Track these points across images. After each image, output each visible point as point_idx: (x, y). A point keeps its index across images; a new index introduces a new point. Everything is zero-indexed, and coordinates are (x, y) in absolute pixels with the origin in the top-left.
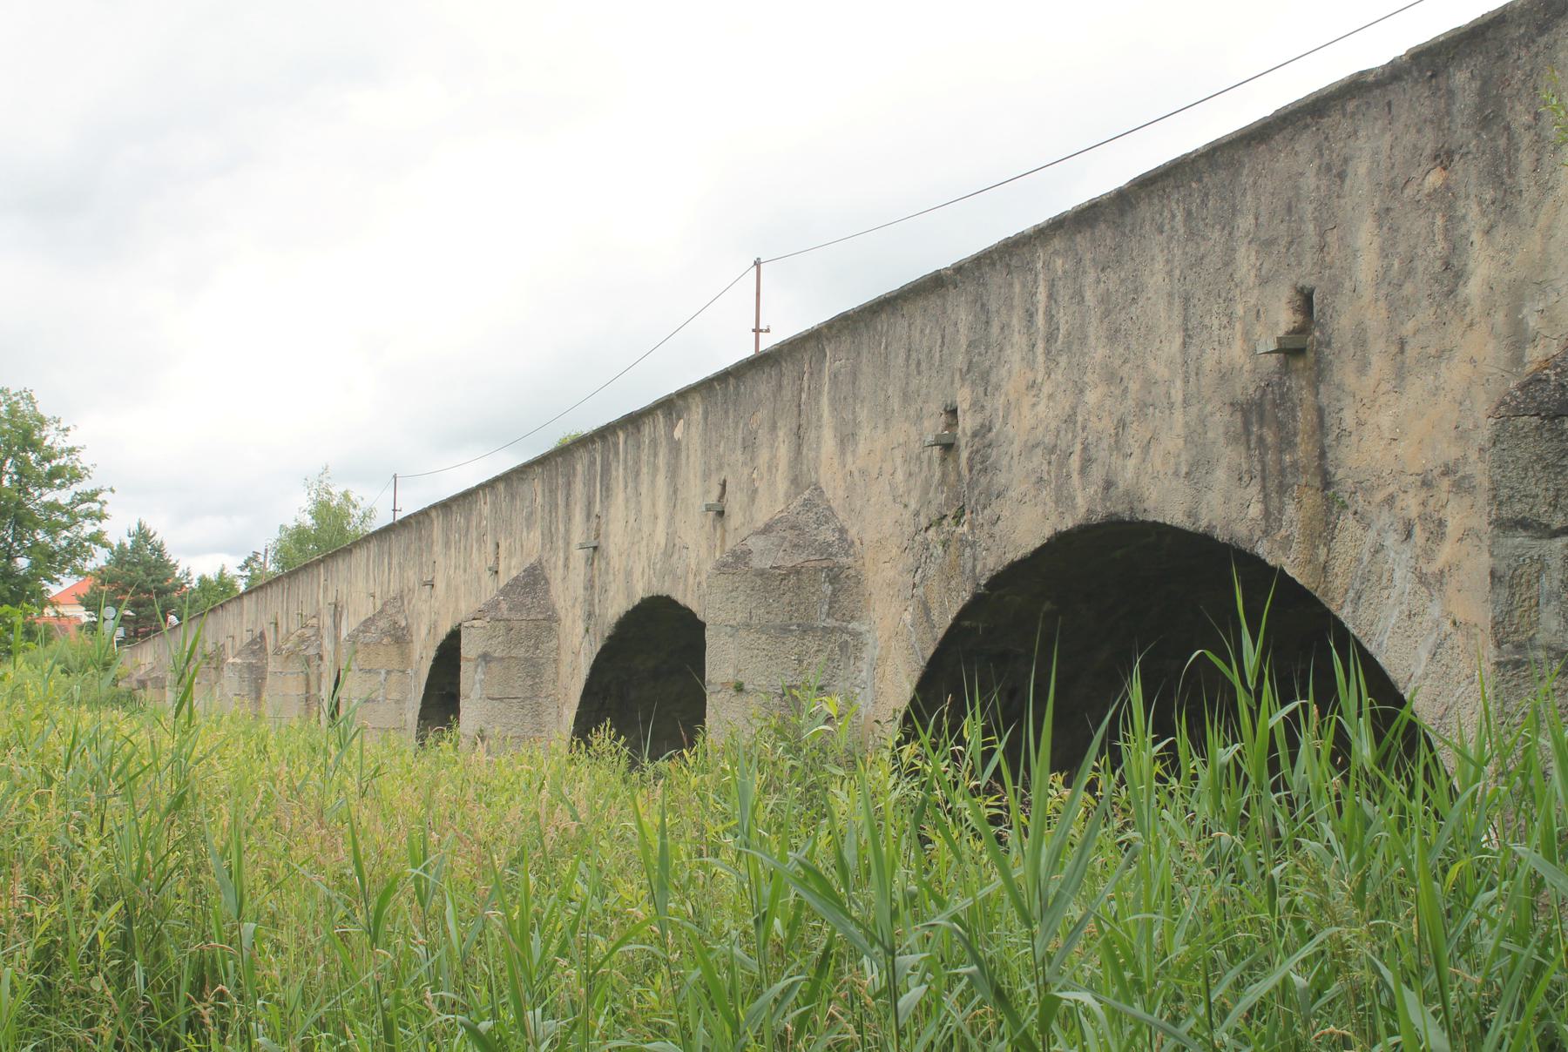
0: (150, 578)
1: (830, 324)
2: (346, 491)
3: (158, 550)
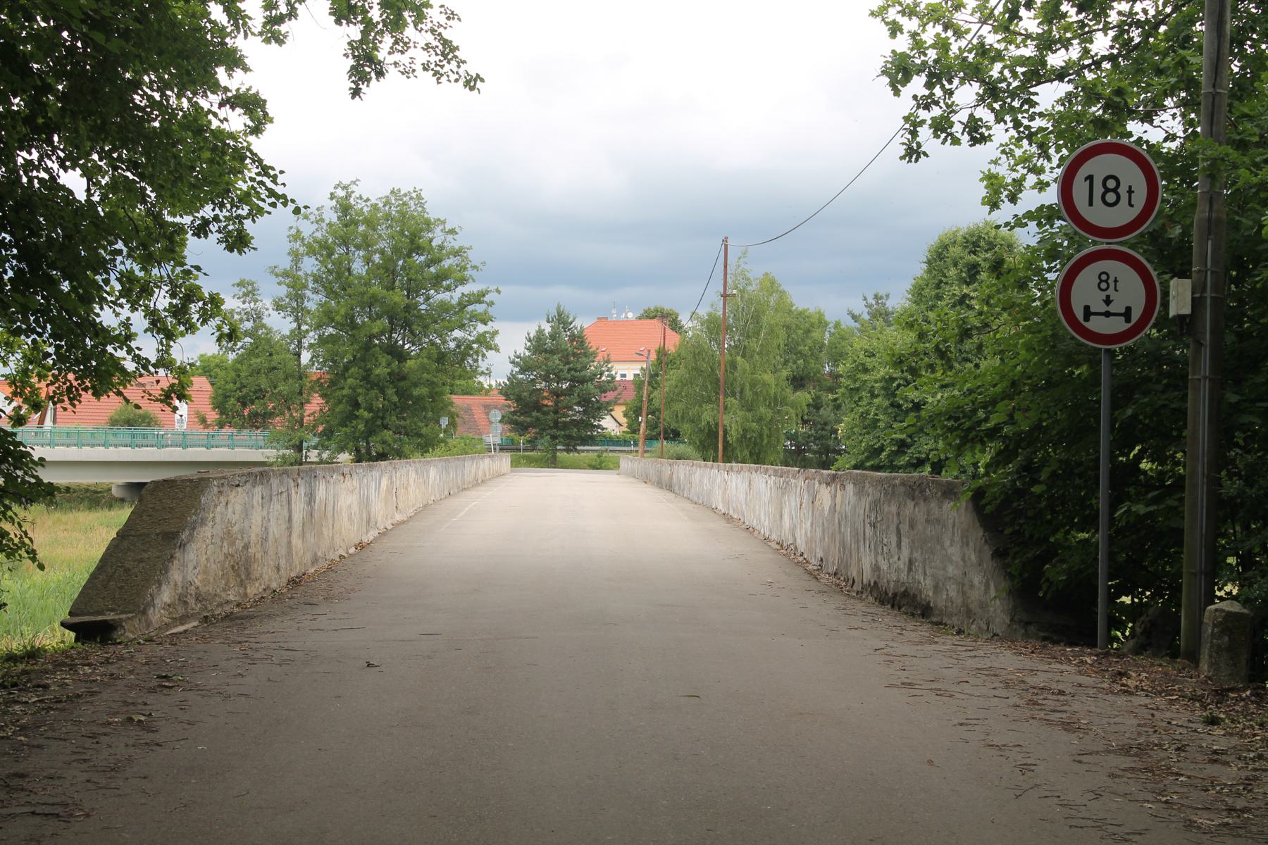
0: (567, 366)
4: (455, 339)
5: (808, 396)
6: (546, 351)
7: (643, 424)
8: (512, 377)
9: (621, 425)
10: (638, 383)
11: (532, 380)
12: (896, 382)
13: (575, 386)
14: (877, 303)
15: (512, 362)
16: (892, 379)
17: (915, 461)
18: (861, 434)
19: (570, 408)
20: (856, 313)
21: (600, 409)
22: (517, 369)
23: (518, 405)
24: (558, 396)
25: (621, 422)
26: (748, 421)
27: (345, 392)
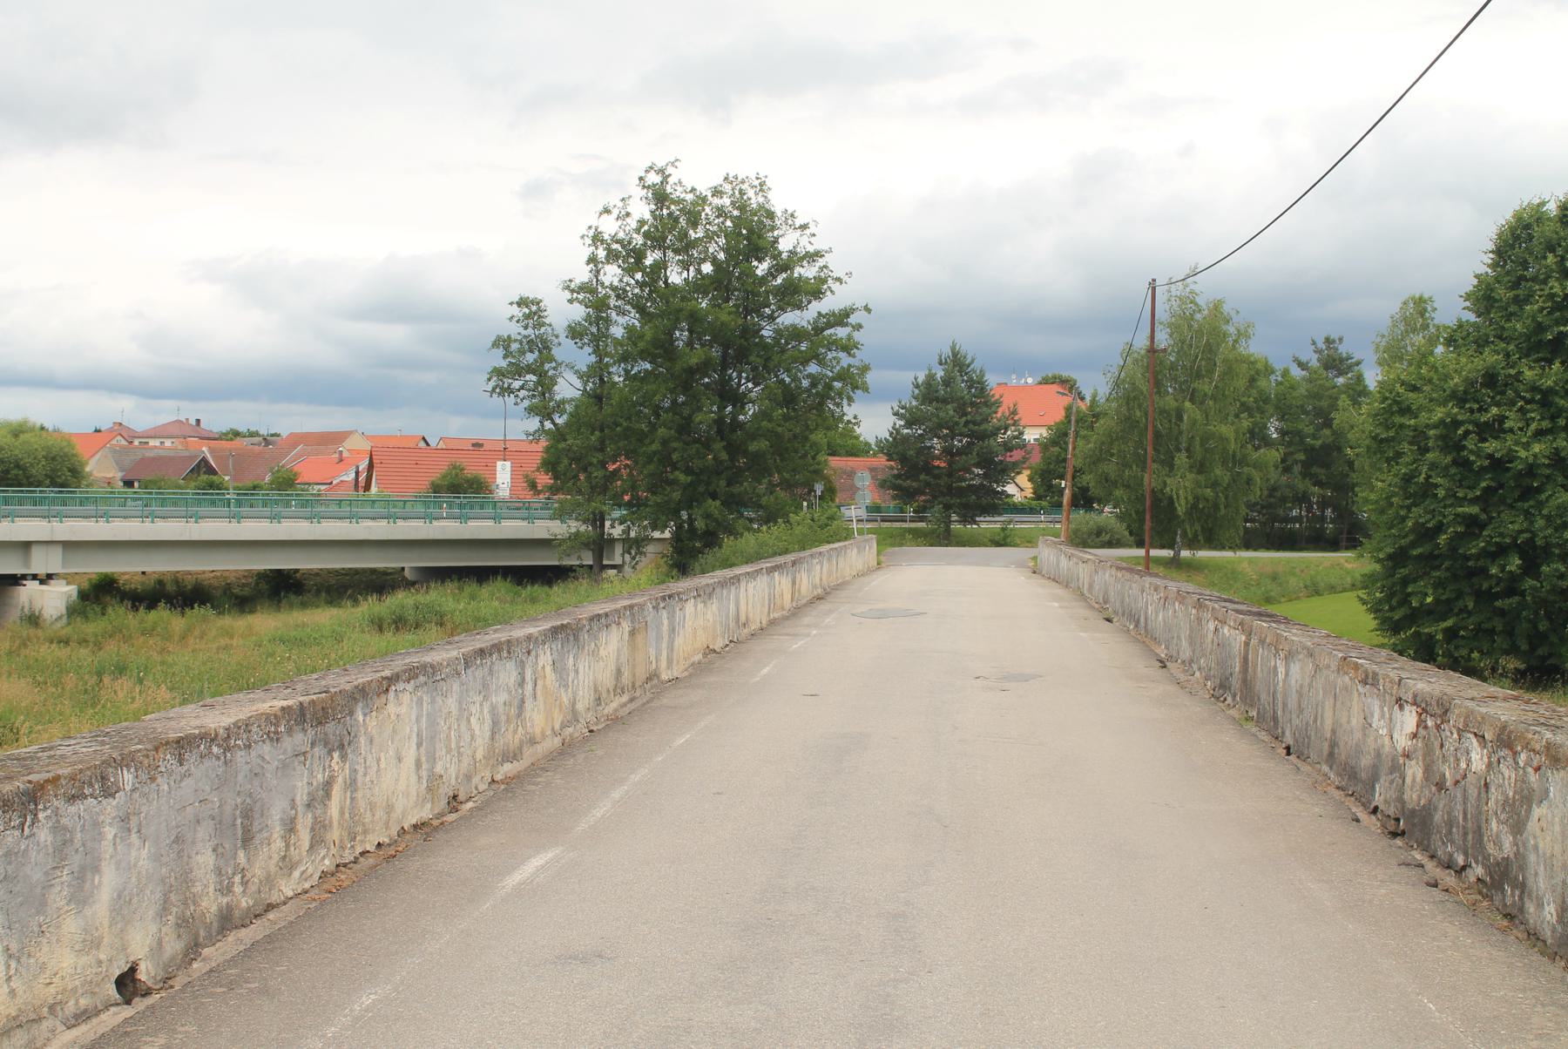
0: (964, 419)
1: (979, 545)
2: (870, 313)
3: (979, 386)
4: (809, 376)
5: (1276, 454)
6: (937, 400)
7: (1067, 491)
8: (895, 432)
9: (1022, 490)
10: (1044, 445)
11: (920, 435)
12: (1463, 428)
13: (973, 443)
14: (1328, 348)
15: (895, 414)
16: (1456, 424)
17: (1493, 549)
18: (1402, 507)
19: (968, 470)
20: (1304, 359)
21: (1003, 471)
22: (902, 423)
23: (902, 468)
24: (952, 455)
25: (1022, 486)
26: (1200, 487)
27: (655, 447)
